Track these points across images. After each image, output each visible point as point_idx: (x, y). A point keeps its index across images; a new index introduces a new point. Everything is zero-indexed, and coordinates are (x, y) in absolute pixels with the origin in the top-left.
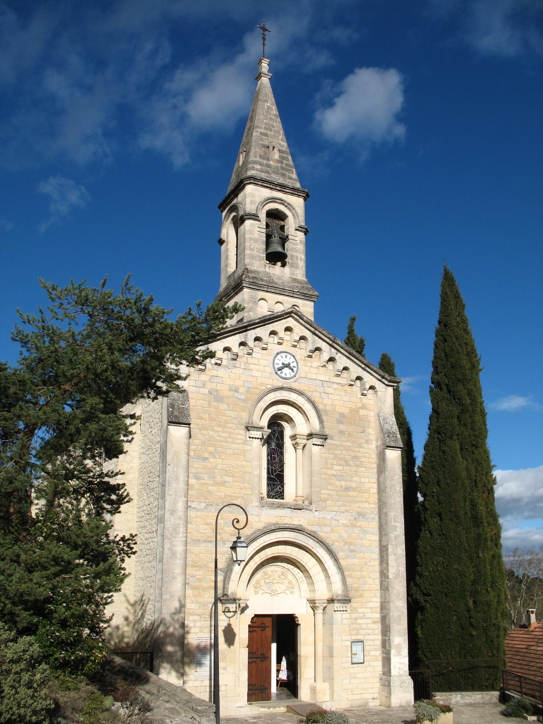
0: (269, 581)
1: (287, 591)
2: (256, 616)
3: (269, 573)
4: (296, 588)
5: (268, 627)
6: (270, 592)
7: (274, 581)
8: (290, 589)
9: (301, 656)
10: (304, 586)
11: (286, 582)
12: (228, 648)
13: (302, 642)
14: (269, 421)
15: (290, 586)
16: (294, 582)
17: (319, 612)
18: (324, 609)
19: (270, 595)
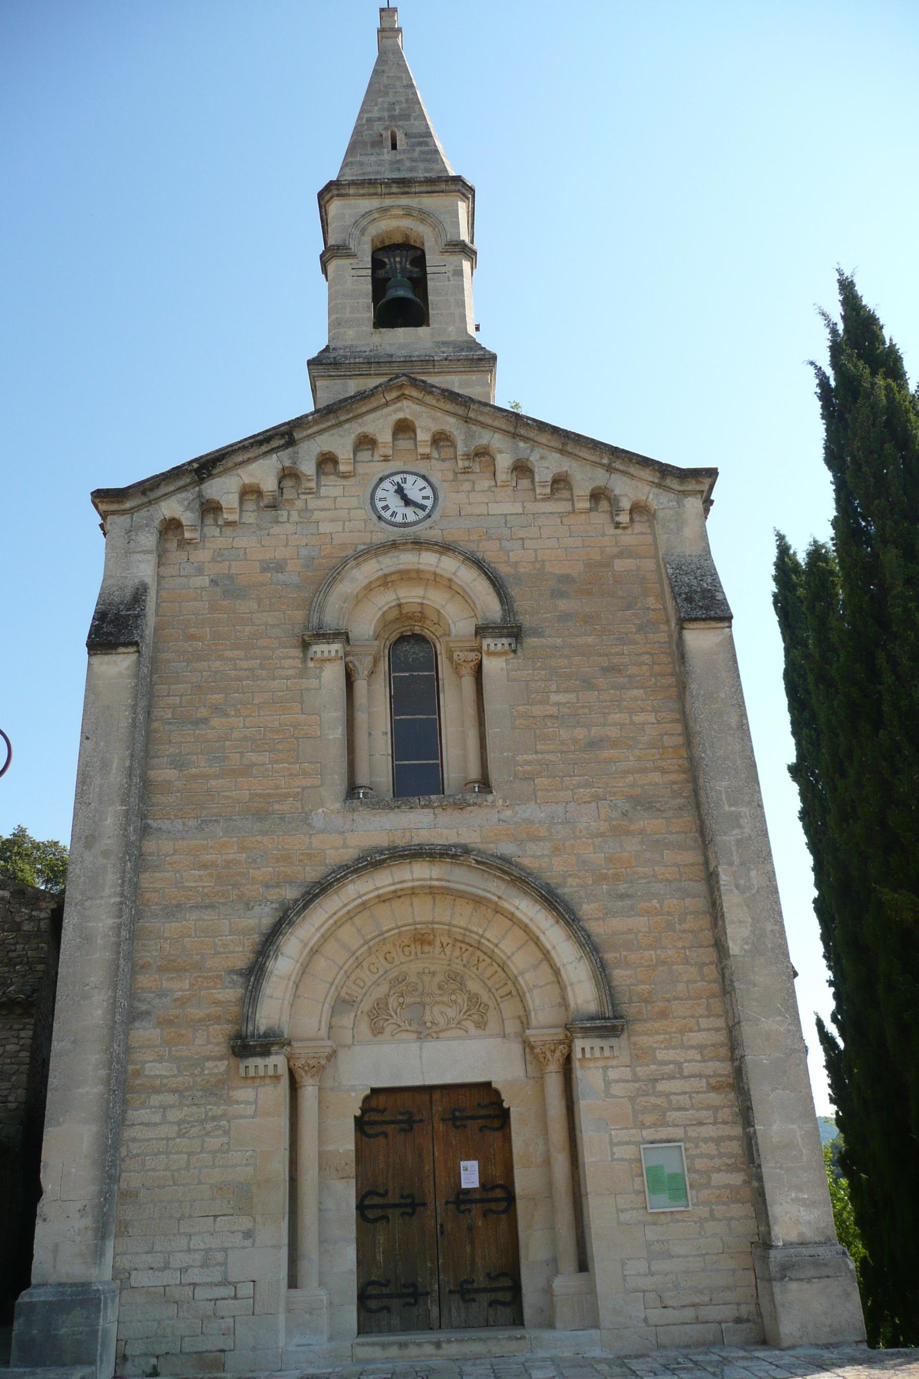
0: (413, 1000)
2: (375, 1091)
4: (492, 1015)
7: (427, 1000)
11: (461, 998)
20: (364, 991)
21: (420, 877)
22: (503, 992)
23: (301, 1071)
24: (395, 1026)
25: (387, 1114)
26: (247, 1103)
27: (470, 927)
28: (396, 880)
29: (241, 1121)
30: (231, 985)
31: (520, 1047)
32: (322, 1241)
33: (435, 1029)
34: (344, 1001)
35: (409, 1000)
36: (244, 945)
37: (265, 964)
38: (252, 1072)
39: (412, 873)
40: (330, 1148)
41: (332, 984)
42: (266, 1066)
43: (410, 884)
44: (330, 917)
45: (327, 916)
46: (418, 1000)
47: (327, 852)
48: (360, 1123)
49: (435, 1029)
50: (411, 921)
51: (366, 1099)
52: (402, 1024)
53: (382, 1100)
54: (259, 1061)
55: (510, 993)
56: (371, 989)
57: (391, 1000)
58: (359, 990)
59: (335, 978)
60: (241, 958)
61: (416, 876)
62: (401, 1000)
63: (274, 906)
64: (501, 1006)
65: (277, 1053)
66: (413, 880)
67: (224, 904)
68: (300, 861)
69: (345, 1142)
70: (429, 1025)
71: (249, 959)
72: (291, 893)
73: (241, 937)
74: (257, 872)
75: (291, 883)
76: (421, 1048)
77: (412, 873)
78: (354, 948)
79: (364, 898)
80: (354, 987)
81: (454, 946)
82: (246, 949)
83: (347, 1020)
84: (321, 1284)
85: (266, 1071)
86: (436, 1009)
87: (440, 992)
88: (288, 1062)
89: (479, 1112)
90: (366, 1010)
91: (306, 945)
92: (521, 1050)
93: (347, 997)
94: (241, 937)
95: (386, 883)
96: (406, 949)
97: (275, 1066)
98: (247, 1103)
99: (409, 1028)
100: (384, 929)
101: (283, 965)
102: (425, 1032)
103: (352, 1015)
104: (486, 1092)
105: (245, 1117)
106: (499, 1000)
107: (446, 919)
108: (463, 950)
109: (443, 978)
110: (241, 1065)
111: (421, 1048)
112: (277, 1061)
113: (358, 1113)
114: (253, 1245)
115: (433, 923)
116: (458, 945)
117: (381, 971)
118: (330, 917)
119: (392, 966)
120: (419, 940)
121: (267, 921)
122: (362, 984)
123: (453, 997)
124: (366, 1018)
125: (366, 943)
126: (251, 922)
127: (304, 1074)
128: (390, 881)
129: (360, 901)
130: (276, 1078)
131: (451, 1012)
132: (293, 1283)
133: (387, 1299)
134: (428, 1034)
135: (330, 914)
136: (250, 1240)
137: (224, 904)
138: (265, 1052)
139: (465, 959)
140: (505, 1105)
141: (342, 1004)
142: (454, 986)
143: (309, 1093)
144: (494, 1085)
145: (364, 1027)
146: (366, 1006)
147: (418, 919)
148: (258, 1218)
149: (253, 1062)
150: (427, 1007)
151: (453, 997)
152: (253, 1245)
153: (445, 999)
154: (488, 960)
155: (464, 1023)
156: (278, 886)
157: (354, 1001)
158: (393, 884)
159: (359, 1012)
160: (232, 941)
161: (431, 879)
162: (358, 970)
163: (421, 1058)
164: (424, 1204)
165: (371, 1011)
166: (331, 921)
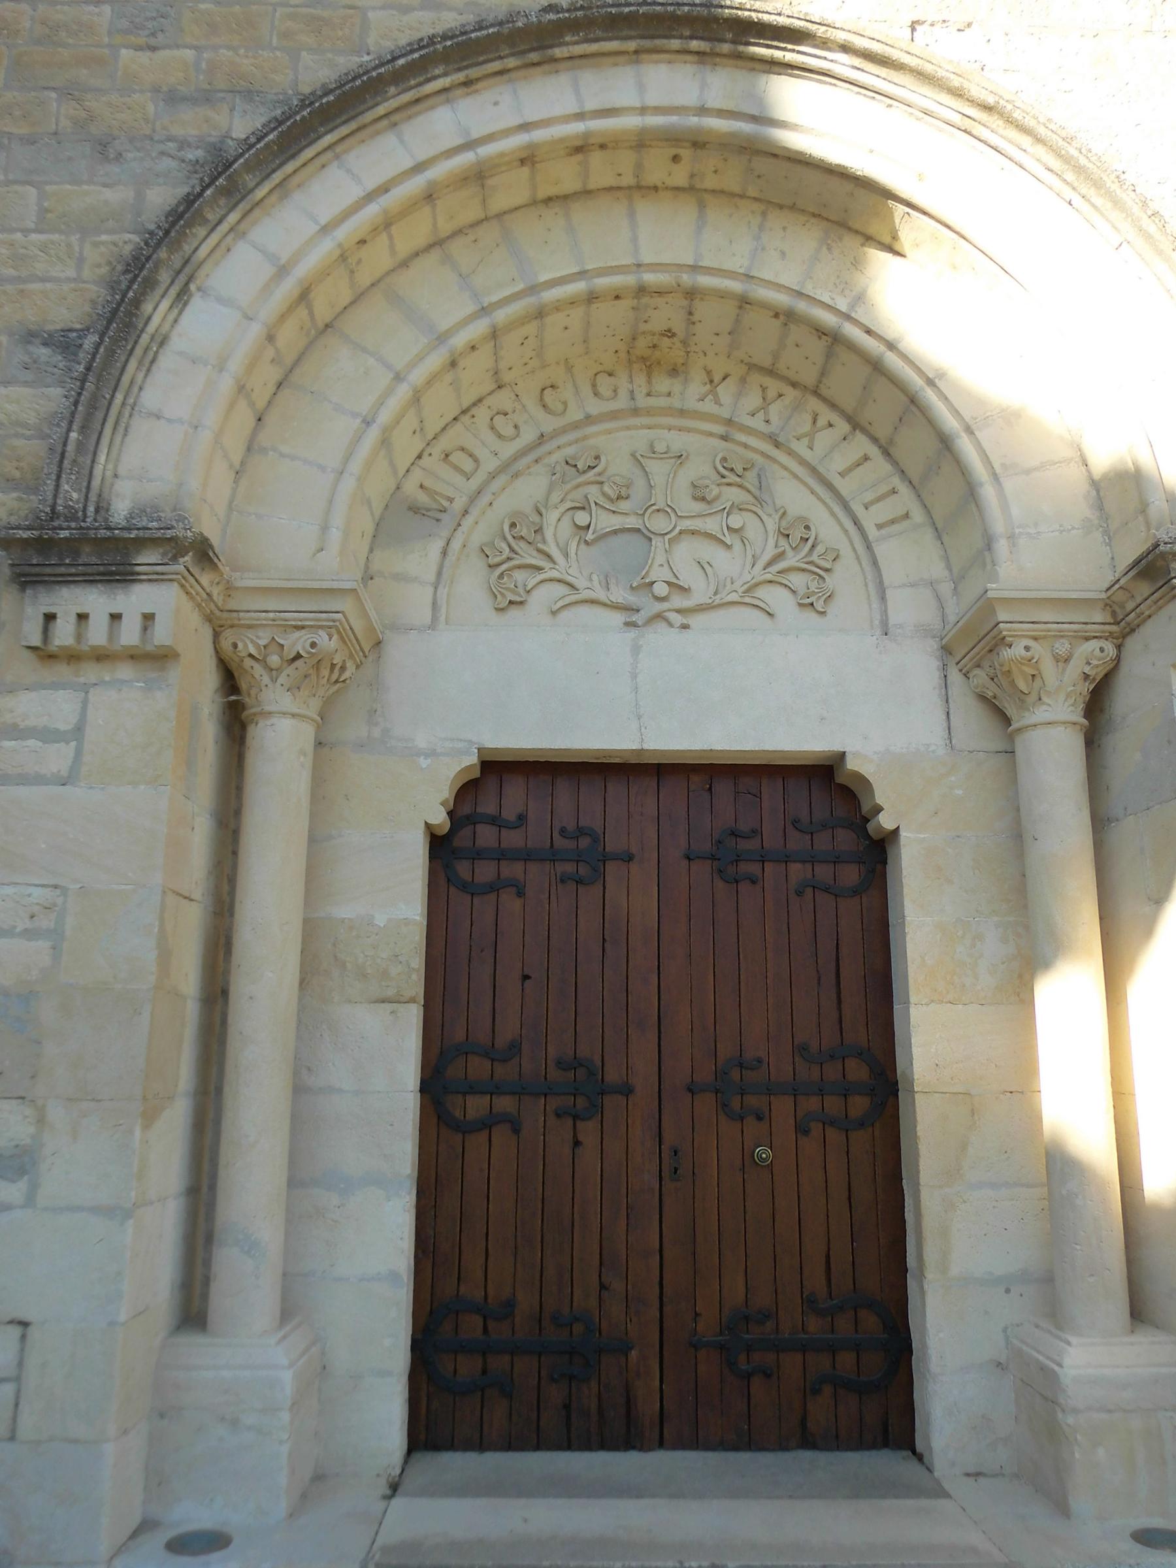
0: (616, 522)
1: (776, 597)
2: (496, 769)
3: (618, 465)
4: (847, 579)
5: (628, 858)
6: (619, 595)
7: (659, 524)
8: (798, 580)
9: (911, 1092)
10: (908, 558)
11: (761, 534)
12: (903, 834)
13: (924, 1177)
14: (870, 784)
15: (792, 560)
16: (828, 529)
17: (1041, 714)
18: (1097, 701)
19: (618, 618)
20: (474, 483)
21: (665, 102)
22: (883, 511)
23: (258, 670)
24: (562, 590)
25: (517, 829)
26: (48, 735)
27: (809, 290)
28: (591, 105)
29: (23, 792)
30: (29, 376)
31: (935, 664)
32: (298, 1180)
33: (678, 601)
34: (415, 509)
35: (605, 522)
36: (81, 260)
37: (137, 303)
38: (64, 634)
39: (641, 87)
40: (345, 912)
41: (367, 423)
42: (116, 617)
43: (632, 122)
44: (370, 197)
45: (357, 192)
46: (632, 522)
47: (370, 14)
48: (440, 846)
49: (678, 601)
50: (627, 260)
51: (467, 790)
52: (580, 583)
53: (515, 797)
54: (96, 601)
55: (907, 516)
56: (496, 485)
57: (552, 516)
58: (459, 479)
59: (380, 403)
60: (67, 289)
61: (652, 99)
62: (582, 518)
63: (191, 155)
64: (879, 550)
65: (158, 579)
66: (643, 110)
67: (29, 141)
68: (286, 35)
69: (392, 901)
70: (661, 589)
71: (93, 302)
72: (241, 123)
73: (74, 239)
74: (144, 57)
75: (249, 94)
76: (636, 650)
77: (641, 87)
78: (444, 325)
79: (485, 151)
80: (445, 472)
81: (743, 380)
82: (86, 273)
83: (421, 560)
84: (288, 1312)
85: (112, 634)
86: (685, 551)
87: (699, 507)
88: (216, 635)
89: (806, 835)
90: (479, 536)
91: (282, 271)
92: (935, 676)
93: (423, 498)
94: (74, 239)
95: (558, 111)
96: (603, 380)
97: (149, 618)
98: (48, 735)
99: (601, 595)
100: (543, 277)
101: (213, 326)
102: (649, 606)
103: (436, 546)
104: (826, 787)
105: (39, 780)
106: (872, 533)
107: (737, 263)
108: (771, 394)
109: (707, 470)
110: (29, 610)
111: (636, 650)
112: (157, 604)
113: (439, 818)
114: (30, 1201)
115: (695, 268)
116: (756, 378)
117: (528, 436)
118: (370, 197)
119: (559, 422)
120: (643, 359)
121: (161, 197)
122: (467, 465)
123: (736, 521)
124: (479, 564)
125: (484, 311)
126: (118, 196)
127: (266, 679)
128: (572, 107)
129: (468, 158)
130: (156, 659)
131: (728, 564)
132: (193, 1311)
133: (499, 1368)
134: (659, 616)
135: (371, 184)
136: (22, 1185)
137: (29, 141)
138: (118, 574)
139: (774, 419)
140: (886, 821)
141: (408, 514)
142: (733, 495)
143: (283, 738)
144: (851, 764)
145: (471, 583)
146: (481, 528)
147: (647, 258)
148: (56, 1113)
149: (69, 601)
150: (657, 541)
151: (736, 521)
152: (30, 1201)
153: (712, 525)
154: (845, 427)
155: (763, 593)
156: (206, 97)
157: (444, 510)
158: (580, 116)
159: (456, 545)
160: (44, 248)
161: (702, 111)
162: (458, 427)
163: (634, 676)
164: (627, 1090)
165: (492, 544)
166: (372, 210)
